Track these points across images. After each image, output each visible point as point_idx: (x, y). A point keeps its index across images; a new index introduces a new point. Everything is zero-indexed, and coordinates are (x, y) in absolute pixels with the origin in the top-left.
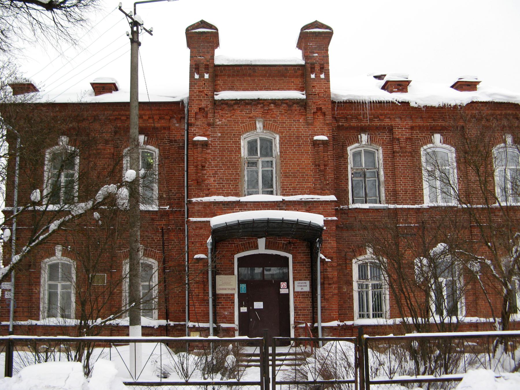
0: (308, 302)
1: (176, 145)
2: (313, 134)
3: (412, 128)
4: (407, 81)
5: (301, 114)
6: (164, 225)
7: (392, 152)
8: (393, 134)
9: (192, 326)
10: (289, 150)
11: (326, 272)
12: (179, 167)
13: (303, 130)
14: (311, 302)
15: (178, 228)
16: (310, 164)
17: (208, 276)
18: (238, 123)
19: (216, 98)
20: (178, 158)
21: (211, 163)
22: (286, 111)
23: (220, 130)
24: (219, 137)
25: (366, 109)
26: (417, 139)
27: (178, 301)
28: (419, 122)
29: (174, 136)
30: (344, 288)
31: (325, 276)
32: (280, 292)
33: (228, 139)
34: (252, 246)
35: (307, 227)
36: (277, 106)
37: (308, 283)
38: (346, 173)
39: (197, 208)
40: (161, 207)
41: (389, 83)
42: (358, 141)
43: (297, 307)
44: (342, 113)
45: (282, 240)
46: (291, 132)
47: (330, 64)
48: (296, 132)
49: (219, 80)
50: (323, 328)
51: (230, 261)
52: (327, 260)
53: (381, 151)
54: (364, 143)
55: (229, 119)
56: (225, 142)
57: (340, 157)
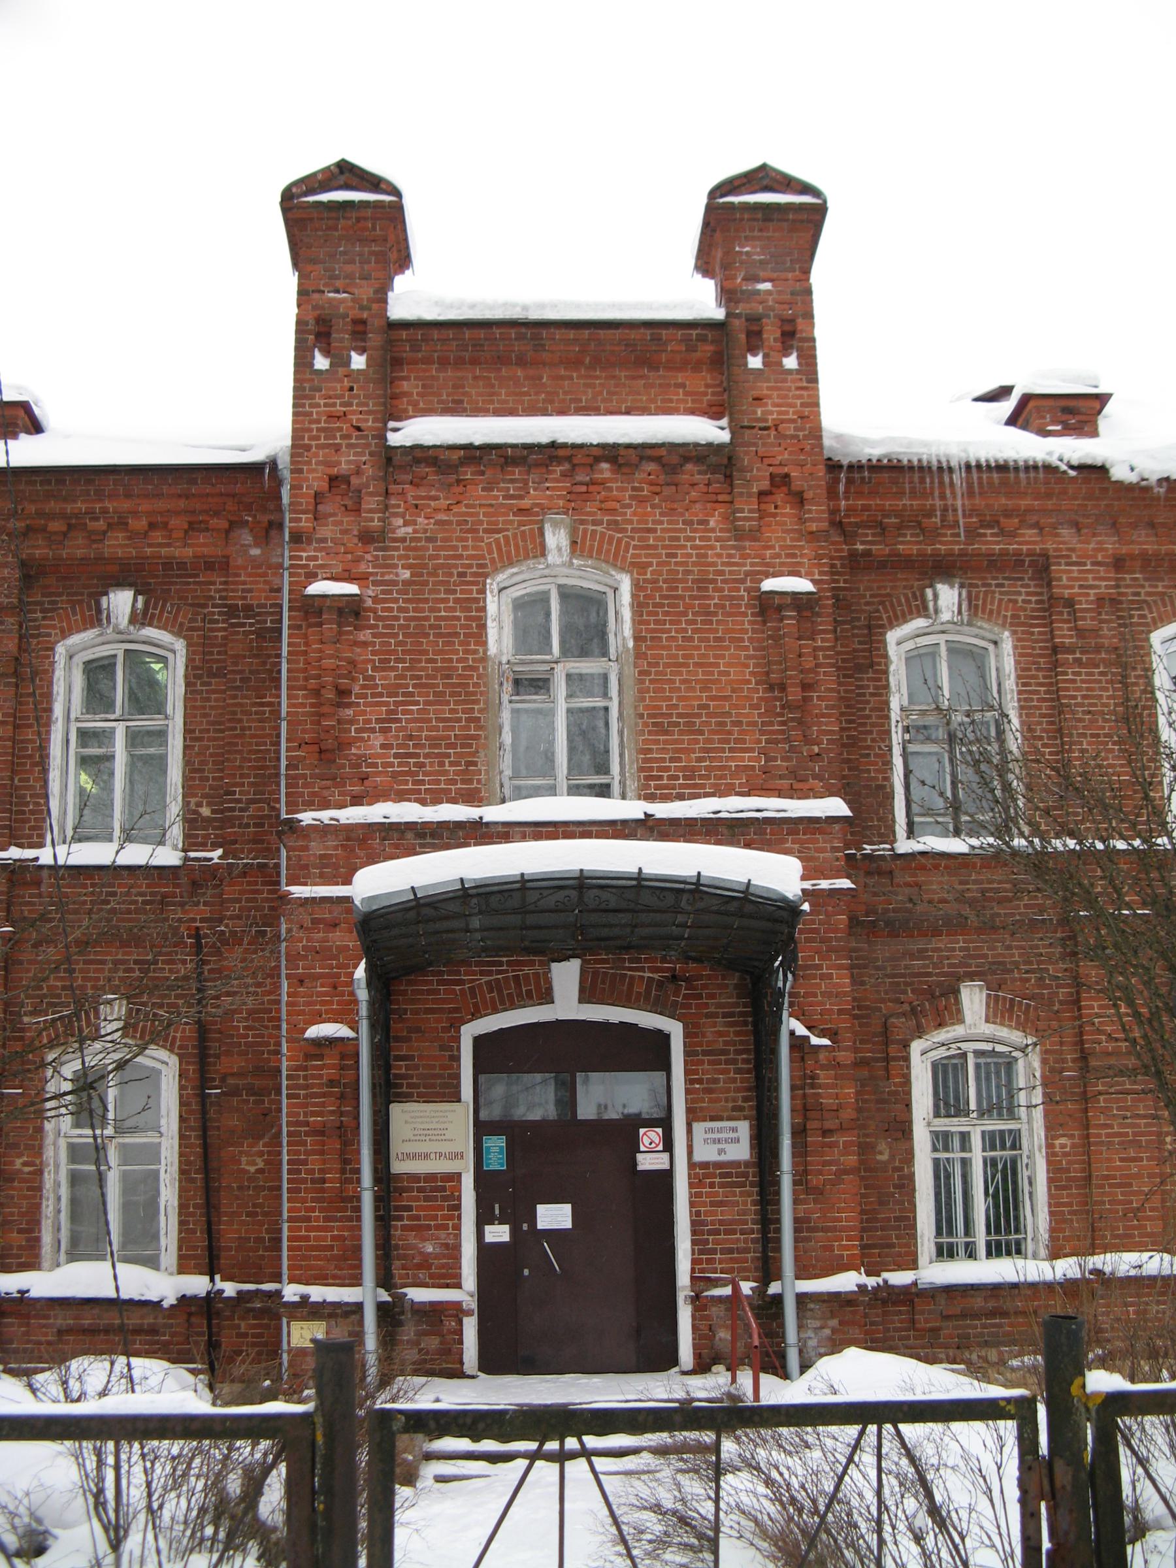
0: (745, 1203)
1: (251, 625)
2: (759, 573)
3: (1119, 563)
4: (1097, 397)
5: (714, 497)
6: (202, 920)
7: (1046, 648)
8: (1049, 585)
9: (297, 1299)
10: (669, 631)
11: (813, 1086)
12: (262, 704)
13: (719, 556)
14: (754, 1203)
15: (254, 929)
16: (748, 682)
17: (357, 1106)
18: (476, 531)
19: (394, 439)
20: (258, 672)
21: (373, 678)
22: (658, 489)
23: (407, 557)
24: (405, 582)
25: (953, 493)
26: (1138, 602)
27: (254, 1205)
28: (1144, 542)
29: (243, 591)
30: (879, 1148)
31: (810, 1100)
32: (635, 1164)
33: (439, 592)
34: (529, 992)
35: (735, 904)
36: (624, 470)
37: (744, 1128)
38: (883, 725)
39: (316, 848)
40: (192, 854)
41: (1031, 404)
42: (926, 608)
43: (703, 1223)
44: (865, 508)
45: (642, 969)
46: (676, 564)
47: (817, 320)
48: (695, 564)
49: (407, 378)
50: (802, 1298)
51: (442, 1048)
52: (815, 1041)
53: (1007, 645)
54: (945, 616)
55: (442, 517)
56: (426, 601)
57: (860, 668)
